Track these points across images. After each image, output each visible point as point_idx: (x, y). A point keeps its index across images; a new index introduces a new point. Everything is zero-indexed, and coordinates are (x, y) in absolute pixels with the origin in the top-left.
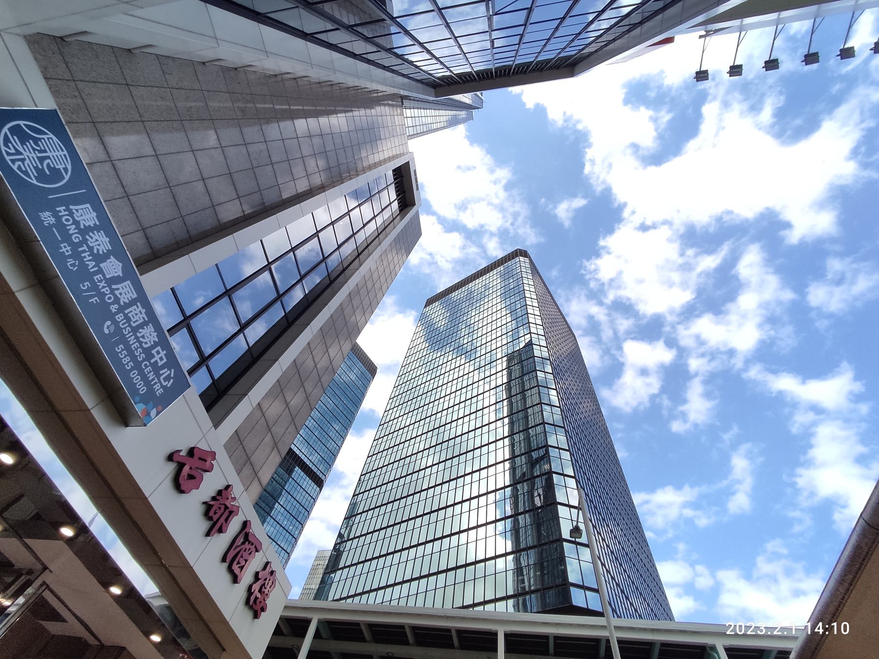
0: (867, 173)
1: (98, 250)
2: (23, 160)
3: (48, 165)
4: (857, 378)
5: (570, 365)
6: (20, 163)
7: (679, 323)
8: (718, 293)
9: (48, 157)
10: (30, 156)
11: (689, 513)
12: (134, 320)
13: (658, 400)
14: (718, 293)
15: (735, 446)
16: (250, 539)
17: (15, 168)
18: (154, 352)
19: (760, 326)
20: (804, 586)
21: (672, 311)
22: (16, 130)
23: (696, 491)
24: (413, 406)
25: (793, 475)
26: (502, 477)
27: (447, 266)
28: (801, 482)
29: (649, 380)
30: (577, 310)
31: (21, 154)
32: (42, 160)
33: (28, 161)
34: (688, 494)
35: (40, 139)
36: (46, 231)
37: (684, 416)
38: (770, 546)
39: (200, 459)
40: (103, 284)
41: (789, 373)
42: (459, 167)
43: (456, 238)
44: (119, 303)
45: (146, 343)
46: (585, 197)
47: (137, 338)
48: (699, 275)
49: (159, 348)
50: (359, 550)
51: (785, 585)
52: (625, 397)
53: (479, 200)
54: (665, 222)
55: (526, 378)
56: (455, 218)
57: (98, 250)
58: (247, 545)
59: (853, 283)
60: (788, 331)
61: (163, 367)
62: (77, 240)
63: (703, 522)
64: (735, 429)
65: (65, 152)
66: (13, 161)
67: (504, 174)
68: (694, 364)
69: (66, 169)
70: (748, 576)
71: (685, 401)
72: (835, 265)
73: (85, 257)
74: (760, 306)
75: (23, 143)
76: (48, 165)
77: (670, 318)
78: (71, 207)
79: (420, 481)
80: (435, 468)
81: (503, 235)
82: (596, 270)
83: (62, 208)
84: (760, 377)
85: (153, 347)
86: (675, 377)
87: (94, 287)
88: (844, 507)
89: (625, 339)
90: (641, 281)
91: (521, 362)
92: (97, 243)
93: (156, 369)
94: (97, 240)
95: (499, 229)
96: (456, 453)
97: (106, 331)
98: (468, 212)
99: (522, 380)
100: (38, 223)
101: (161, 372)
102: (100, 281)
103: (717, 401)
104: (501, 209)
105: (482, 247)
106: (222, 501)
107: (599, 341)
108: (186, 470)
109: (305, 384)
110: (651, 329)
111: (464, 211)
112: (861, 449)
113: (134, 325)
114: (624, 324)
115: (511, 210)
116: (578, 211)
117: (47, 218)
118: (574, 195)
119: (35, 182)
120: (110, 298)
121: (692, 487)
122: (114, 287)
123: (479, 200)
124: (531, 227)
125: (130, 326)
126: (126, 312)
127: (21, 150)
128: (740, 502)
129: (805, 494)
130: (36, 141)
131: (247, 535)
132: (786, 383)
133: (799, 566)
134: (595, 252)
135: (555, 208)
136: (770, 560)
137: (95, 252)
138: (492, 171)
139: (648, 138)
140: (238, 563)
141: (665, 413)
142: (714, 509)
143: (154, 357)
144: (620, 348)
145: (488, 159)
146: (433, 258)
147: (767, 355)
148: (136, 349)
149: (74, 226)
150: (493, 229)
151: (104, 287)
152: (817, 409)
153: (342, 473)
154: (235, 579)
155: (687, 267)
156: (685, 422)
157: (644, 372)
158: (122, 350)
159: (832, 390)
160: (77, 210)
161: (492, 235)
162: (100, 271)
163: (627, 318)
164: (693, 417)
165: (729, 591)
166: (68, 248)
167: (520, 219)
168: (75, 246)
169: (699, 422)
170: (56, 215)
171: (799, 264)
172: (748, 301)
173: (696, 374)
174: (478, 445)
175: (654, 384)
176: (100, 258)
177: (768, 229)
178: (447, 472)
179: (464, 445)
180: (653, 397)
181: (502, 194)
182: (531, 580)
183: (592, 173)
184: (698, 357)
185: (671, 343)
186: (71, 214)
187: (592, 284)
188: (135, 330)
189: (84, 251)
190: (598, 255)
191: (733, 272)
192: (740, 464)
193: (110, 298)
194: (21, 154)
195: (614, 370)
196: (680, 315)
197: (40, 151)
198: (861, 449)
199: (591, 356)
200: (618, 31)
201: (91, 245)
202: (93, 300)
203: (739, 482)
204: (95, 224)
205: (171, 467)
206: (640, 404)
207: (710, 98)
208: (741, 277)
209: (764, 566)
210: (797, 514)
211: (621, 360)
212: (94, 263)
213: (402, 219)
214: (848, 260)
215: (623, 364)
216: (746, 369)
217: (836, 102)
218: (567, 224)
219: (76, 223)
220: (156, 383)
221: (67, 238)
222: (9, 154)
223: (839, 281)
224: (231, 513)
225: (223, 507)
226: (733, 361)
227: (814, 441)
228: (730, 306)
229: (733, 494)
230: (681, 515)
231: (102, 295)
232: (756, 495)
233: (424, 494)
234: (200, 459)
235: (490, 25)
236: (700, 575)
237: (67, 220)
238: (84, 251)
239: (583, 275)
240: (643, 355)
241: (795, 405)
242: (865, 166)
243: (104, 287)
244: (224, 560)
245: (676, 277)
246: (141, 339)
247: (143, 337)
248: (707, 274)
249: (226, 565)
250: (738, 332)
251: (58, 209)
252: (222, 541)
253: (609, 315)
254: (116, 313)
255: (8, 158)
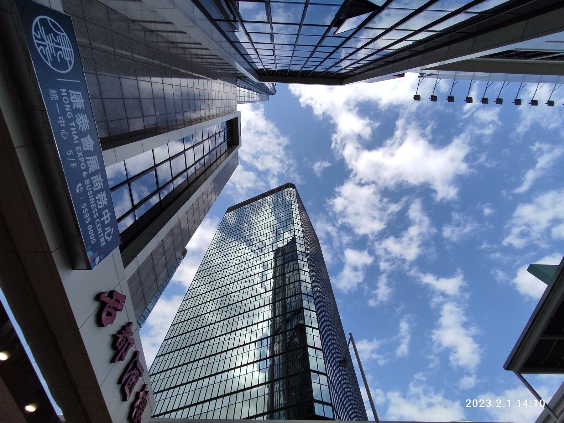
0: (471, 170)
1: (81, 128)
2: (45, 46)
3: (60, 55)
4: (464, 279)
5: (316, 260)
6: (43, 48)
7: (376, 241)
8: (397, 226)
9: (61, 50)
10: (50, 44)
11: (374, 356)
12: (95, 186)
13: (362, 285)
14: (397, 226)
15: (401, 316)
16: (138, 366)
17: (39, 50)
18: (104, 212)
19: (419, 246)
20: (433, 400)
21: (372, 233)
22: (43, 22)
23: (379, 342)
24: (210, 279)
25: (430, 333)
26: (264, 329)
27: (243, 192)
28: (434, 337)
29: (357, 274)
30: (321, 228)
31: (44, 41)
32: (57, 50)
33: (47, 48)
34: (375, 344)
35: (58, 35)
36: (52, 103)
37: (376, 296)
38: (416, 376)
39: (116, 300)
40: (80, 154)
41: (431, 273)
42: (257, 132)
43: (251, 175)
44: (88, 171)
45: (100, 205)
46: (330, 162)
47: (95, 200)
48: (389, 215)
49: (107, 210)
50: (165, 380)
51: (424, 400)
52: (344, 282)
53: (268, 154)
54: (373, 182)
55: (286, 265)
56: (251, 163)
57: (81, 128)
58: (135, 371)
59: (465, 226)
60: (433, 250)
61: (107, 225)
62: (69, 117)
63: (382, 362)
64: (403, 306)
65: (72, 50)
66: (39, 45)
67: (285, 141)
68: (383, 265)
69: (70, 62)
70: (405, 395)
71: (377, 288)
72: (456, 216)
73: (73, 131)
74: (420, 234)
75: (47, 34)
76: (60, 55)
77: (371, 237)
78: (70, 91)
79: (215, 331)
80: (221, 323)
81: (280, 176)
82: (333, 206)
83: (64, 90)
84: (417, 275)
85: (104, 209)
86: (372, 273)
87: (75, 155)
88: (455, 353)
89: (346, 248)
90: (357, 214)
91: (284, 255)
92: (81, 122)
93: (104, 226)
94: (81, 120)
95: (278, 173)
96: (242, 311)
97: (78, 191)
98: (260, 160)
99: (284, 266)
100: (48, 96)
101: (106, 229)
102: (79, 152)
103: (462, 277)
104: (282, 161)
105: (267, 183)
106: (124, 335)
107: (332, 248)
108: (107, 309)
109: (166, 254)
110: (361, 243)
111: (257, 160)
112: (464, 319)
113: (95, 190)
114: (346, 239)
115: (287, 162)
116: (326, 169)
117: (53, 92)
118: (324, 160)
119: (50, 65)
120: (83, 166)
121: (377, 340)
122: (87, 158)
123: (268, 154)
124: (298, 174)
125: (92, 190)
126: (92, 178)
127: (45, 38)
128: (403, 349)
129: (436, 344)
130: (56, 35)
131: (136, 362)
132: (428, 279)
133: (431, 389)
134: (333, 195)
135: (313, 165)
136: (416, 386)
137: (79, 129)
138: (278, 138)
139: (367, 132)
140: (129, 385)
141: (365, 294)
142: (389, 353)
143: (103, 217)
144: (343, 254)
145: (276, 130)
146: (235, 186)
147: (421, 263)
148: (94, 209)
149: (69, 106)
150: (275, 173)
151: (81, 157)
152: (444, 294)
153: (153, 326)
154: (124, 398)
155: (383, 209)
156: (376, 300)
157: (355, 269)
158: (86, 208)
159: (450, 285)
160: (73, 94)
161: (274, 176)
162: (80, 144)
163: (348, 236)
164: (380, 297)
165: (394, 405)
166: (63, 121)
167: (292, 168)
168: (68, 121)
169: (384, 300)
170: (59, 93)
171: (439, 212)
172: (413, 231)
173: (384, 272)
174: (257, 306)
175: (360, 277)
176: (82, 134)
177: (425, 191)
178: (230, 326)
179: (248, 306)
180: (359, 284)
181: (282, 152)
182: (279, 400)
183: (335, 148)
184: (385, 262)
185: (372, 253)
186: (69, 96)
187: (330, 213)
188: (95, 193)
189: (73, 126)
190: (335, 197)
191: (406, 214)
192: (404, 326)
193: (83, 166)
194: (44, 41)
195: (340, 266)
196: (376, 236)
197: (57, 44)
198: (464, 319)
199: (327, 257)
200: (363, 69)
201: (78, 123)
202: (73, 165)
203: (403, 338)
204: (82, 108)
205: (95, 306)
206: (352, 288)
207: (400, 116)
208: (410, 217)
209: (413, 390)
210: (432, 357)
211: (344, 261)
212: (77, 137)
213: (228, 154)
214: (462, 214)
215: (344, 263)
216: (409, 270)
217: (459, 132)
218: (319, 175)
219: (71, 104)
220: (102, 237)
221: (64, 113)
222: (36, 38)
223: (458, 225)
224: (129, 344)
225: (125, 339)
226: (403, 266)
227: (442, 313)
228: (404, 233)
229: (400, 345)
230: (370, 358)
231: (79, 163)
232: (411, 345)
233: (217, 339)
234: (116, 300)
235: (293, 54)
236: (378, 395)
237: (66, 100)
238: (73, 126)
239: (325, 208)
240: (352, 256)
241: (433, 292)
242: (471, 167)
243: (81, 157)
244: (119, 382)
245: (376, 214)
246: (98, 201)
247: (99, 200)
248: (392, 214)
249: (120, 385)
250: (407, 248)
251: (61, 90)
252: (121, 365)
253: (338, 233)
254: (86, 178)
255: (35, 41)
